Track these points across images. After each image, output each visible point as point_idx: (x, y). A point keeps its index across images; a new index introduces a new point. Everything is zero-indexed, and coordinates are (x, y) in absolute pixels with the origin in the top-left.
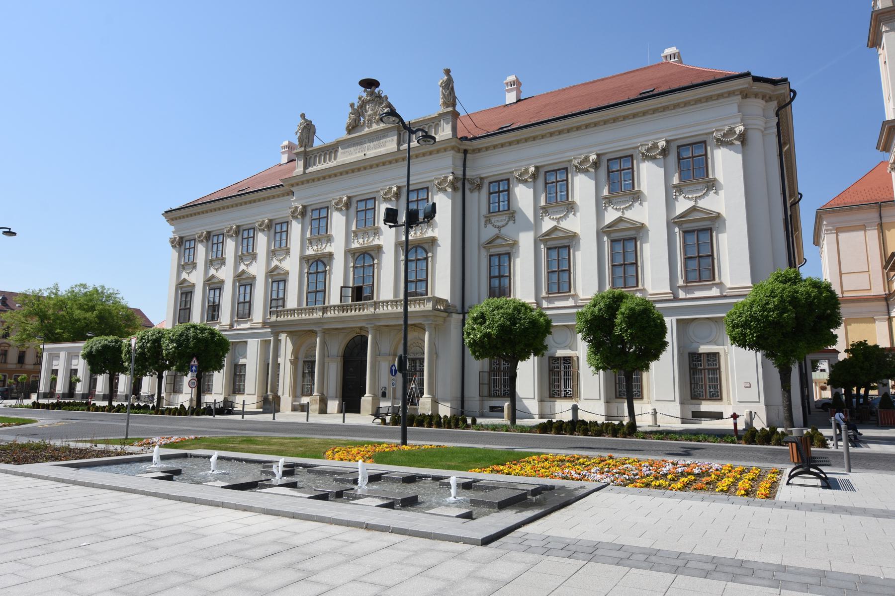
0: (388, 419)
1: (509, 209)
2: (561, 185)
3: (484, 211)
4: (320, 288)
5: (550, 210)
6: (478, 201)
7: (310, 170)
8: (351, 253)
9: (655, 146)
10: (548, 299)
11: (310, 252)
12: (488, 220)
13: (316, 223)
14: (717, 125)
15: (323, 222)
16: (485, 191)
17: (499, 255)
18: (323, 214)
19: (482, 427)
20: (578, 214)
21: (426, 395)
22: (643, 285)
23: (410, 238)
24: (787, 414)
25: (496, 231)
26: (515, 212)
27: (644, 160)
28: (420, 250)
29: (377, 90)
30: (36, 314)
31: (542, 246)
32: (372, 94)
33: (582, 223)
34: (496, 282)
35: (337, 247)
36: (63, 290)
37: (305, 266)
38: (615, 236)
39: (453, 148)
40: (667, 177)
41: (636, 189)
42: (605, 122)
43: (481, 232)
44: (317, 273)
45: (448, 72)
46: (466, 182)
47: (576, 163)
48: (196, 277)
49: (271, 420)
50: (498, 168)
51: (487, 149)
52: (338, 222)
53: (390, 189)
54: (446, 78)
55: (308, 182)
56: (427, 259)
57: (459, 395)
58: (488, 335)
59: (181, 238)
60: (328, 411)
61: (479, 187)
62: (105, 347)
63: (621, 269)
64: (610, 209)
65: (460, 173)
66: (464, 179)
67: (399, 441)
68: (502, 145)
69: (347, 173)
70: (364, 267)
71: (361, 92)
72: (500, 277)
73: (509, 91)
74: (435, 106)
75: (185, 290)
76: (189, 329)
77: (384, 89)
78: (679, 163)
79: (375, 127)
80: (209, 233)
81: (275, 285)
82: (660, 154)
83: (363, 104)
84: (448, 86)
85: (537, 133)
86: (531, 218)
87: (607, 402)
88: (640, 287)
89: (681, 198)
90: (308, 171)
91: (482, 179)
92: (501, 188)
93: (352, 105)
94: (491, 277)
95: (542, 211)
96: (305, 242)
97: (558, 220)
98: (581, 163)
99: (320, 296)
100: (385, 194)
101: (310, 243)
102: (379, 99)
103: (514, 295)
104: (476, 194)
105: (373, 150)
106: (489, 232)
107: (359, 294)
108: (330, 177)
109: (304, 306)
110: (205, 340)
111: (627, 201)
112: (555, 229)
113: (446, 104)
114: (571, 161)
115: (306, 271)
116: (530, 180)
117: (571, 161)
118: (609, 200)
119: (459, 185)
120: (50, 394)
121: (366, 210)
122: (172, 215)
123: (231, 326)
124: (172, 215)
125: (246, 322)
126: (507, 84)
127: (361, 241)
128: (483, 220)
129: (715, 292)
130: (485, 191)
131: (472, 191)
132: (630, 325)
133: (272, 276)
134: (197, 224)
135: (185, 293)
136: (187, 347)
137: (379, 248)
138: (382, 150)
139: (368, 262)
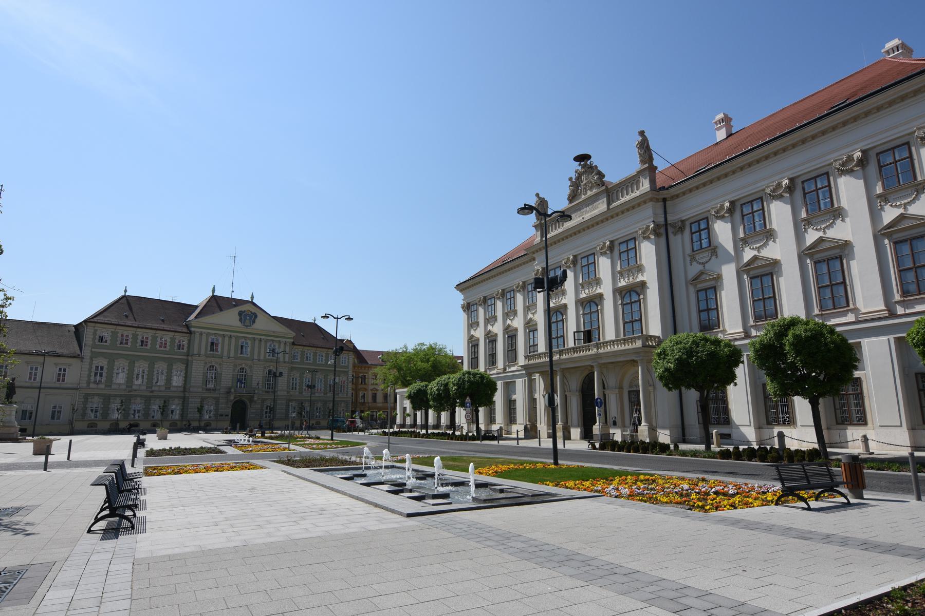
0: (597, 445)
1: (710, 245)
2: (824, 193)
3: (688, 250)
4: (636, 317)
5: (750, 241)
6: (681, 243)
7: (614, 205)
8: (619, 292)
9: (850, 158)
10: (755, 327)
11: (622, 283)
12: (693, 259)
13: (585, 269)
14: (834, 155)
15: (632, 254)
16: (687, 233)
17: (706, 290)
18: (591, 260)
19: (684, 453)
20: (847, 220)
21: (643, 424)
22: (854, 304)
23: (552, 305)
24: (704, 435)
25: (701, 267)
26: (716, 247)
27: (840, 175)
28: (593, 304)
29: (588, 162)
30: (395, 367)
31: (745, 277)
32: (584, 166)
33: (782, 249)
34: (704, 315)
35: (606, 289)
36: (411, 348)
37: (580, 308)
38: (818, 257)
39: (651, 200)
40: (869, 188)
41: (836, 206)
42: (794, 146)
43: (686, 270)
44: (631, 303)
45: (642, 133)
46: (669, 227)
47: (838, 166)
48: (479, 333)
49: (537, 446)
50: (750, 188)
51: (684, 193)
52: (604, 265)
53: (604, 244)
54: (640, 139)
55: (612, 217)
56: (639, 300)
57: (679, 422)
58: (667, 370)
59: (468, 304)
60: (572, 437)
61: (681, 229)
62: (419, 390)
63: (828, 291)
64: (810, 230)
65: (661, 220)
66: (666, 225)
67: (552, 461)
68: (697, 188)
69: (571, 236)
70: (591, 313)
71: (576, 166)
72: (708, 310)
73: (718, 129)
74: (634, 165)
75: (532, 328)
76: (292, 400)
77: (594, 161)
78: (880, 171)
79: (589, 193)
80: (485, 298)
81: (531, 334)
82: (856, 165)
83: (579, 178)
84: (644, 147)
85: (728, 170)
86: (731, 249)
87: (912, 429)
88: (851, 306)
89: (887, 207)
90: (611, 207)
91: (683, 222)
92: (702, 226)
93: (570, 179)
94: (700, 311)
95: (740, 243)
96: (578, 287)
97: (758, 249)
98: (774, 191)
99: (636, 326)
100: (601, 249)
101: (583, 287)
102: (591, 169)
103: (782, 315)
104: (679, 236)
105: (589, 214)
106: (694, 269)
107: (588, 336)
108: (559, 241)
109: (622, 337)
110: (476, 383)
111: (828, 220)
112: (755, 258)
113: (642, 162)
114: (764, 190)
115: (620, 302)
116: (727, 215)
117: (764, 190)
118: (808, 222)
119: (663, 230)
120: (403, 425)
121: (627, 251)
122: (461, 287)
123: (505, 369)
124: (461, 287)
125: (514, 366)
126: (716, 123)
127: (587, 291)
128: (688, 259)
129: (851, 318)
130: (687, 233)
131: (675, 234)
132: (798, 353)
133: (528, 327)
134: (479, 292)
135: (473, 344)
136: (464, 388)
137: (601, 296)
138: (596, 212)
139: (594, 309)
